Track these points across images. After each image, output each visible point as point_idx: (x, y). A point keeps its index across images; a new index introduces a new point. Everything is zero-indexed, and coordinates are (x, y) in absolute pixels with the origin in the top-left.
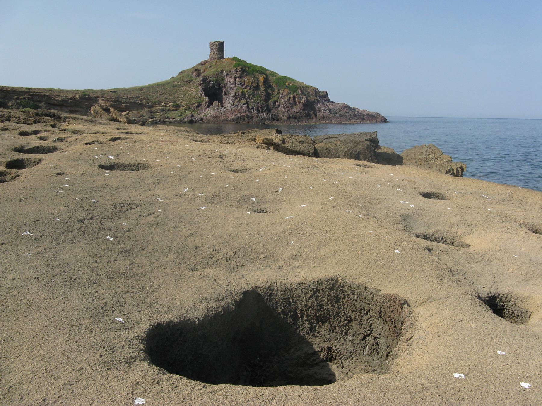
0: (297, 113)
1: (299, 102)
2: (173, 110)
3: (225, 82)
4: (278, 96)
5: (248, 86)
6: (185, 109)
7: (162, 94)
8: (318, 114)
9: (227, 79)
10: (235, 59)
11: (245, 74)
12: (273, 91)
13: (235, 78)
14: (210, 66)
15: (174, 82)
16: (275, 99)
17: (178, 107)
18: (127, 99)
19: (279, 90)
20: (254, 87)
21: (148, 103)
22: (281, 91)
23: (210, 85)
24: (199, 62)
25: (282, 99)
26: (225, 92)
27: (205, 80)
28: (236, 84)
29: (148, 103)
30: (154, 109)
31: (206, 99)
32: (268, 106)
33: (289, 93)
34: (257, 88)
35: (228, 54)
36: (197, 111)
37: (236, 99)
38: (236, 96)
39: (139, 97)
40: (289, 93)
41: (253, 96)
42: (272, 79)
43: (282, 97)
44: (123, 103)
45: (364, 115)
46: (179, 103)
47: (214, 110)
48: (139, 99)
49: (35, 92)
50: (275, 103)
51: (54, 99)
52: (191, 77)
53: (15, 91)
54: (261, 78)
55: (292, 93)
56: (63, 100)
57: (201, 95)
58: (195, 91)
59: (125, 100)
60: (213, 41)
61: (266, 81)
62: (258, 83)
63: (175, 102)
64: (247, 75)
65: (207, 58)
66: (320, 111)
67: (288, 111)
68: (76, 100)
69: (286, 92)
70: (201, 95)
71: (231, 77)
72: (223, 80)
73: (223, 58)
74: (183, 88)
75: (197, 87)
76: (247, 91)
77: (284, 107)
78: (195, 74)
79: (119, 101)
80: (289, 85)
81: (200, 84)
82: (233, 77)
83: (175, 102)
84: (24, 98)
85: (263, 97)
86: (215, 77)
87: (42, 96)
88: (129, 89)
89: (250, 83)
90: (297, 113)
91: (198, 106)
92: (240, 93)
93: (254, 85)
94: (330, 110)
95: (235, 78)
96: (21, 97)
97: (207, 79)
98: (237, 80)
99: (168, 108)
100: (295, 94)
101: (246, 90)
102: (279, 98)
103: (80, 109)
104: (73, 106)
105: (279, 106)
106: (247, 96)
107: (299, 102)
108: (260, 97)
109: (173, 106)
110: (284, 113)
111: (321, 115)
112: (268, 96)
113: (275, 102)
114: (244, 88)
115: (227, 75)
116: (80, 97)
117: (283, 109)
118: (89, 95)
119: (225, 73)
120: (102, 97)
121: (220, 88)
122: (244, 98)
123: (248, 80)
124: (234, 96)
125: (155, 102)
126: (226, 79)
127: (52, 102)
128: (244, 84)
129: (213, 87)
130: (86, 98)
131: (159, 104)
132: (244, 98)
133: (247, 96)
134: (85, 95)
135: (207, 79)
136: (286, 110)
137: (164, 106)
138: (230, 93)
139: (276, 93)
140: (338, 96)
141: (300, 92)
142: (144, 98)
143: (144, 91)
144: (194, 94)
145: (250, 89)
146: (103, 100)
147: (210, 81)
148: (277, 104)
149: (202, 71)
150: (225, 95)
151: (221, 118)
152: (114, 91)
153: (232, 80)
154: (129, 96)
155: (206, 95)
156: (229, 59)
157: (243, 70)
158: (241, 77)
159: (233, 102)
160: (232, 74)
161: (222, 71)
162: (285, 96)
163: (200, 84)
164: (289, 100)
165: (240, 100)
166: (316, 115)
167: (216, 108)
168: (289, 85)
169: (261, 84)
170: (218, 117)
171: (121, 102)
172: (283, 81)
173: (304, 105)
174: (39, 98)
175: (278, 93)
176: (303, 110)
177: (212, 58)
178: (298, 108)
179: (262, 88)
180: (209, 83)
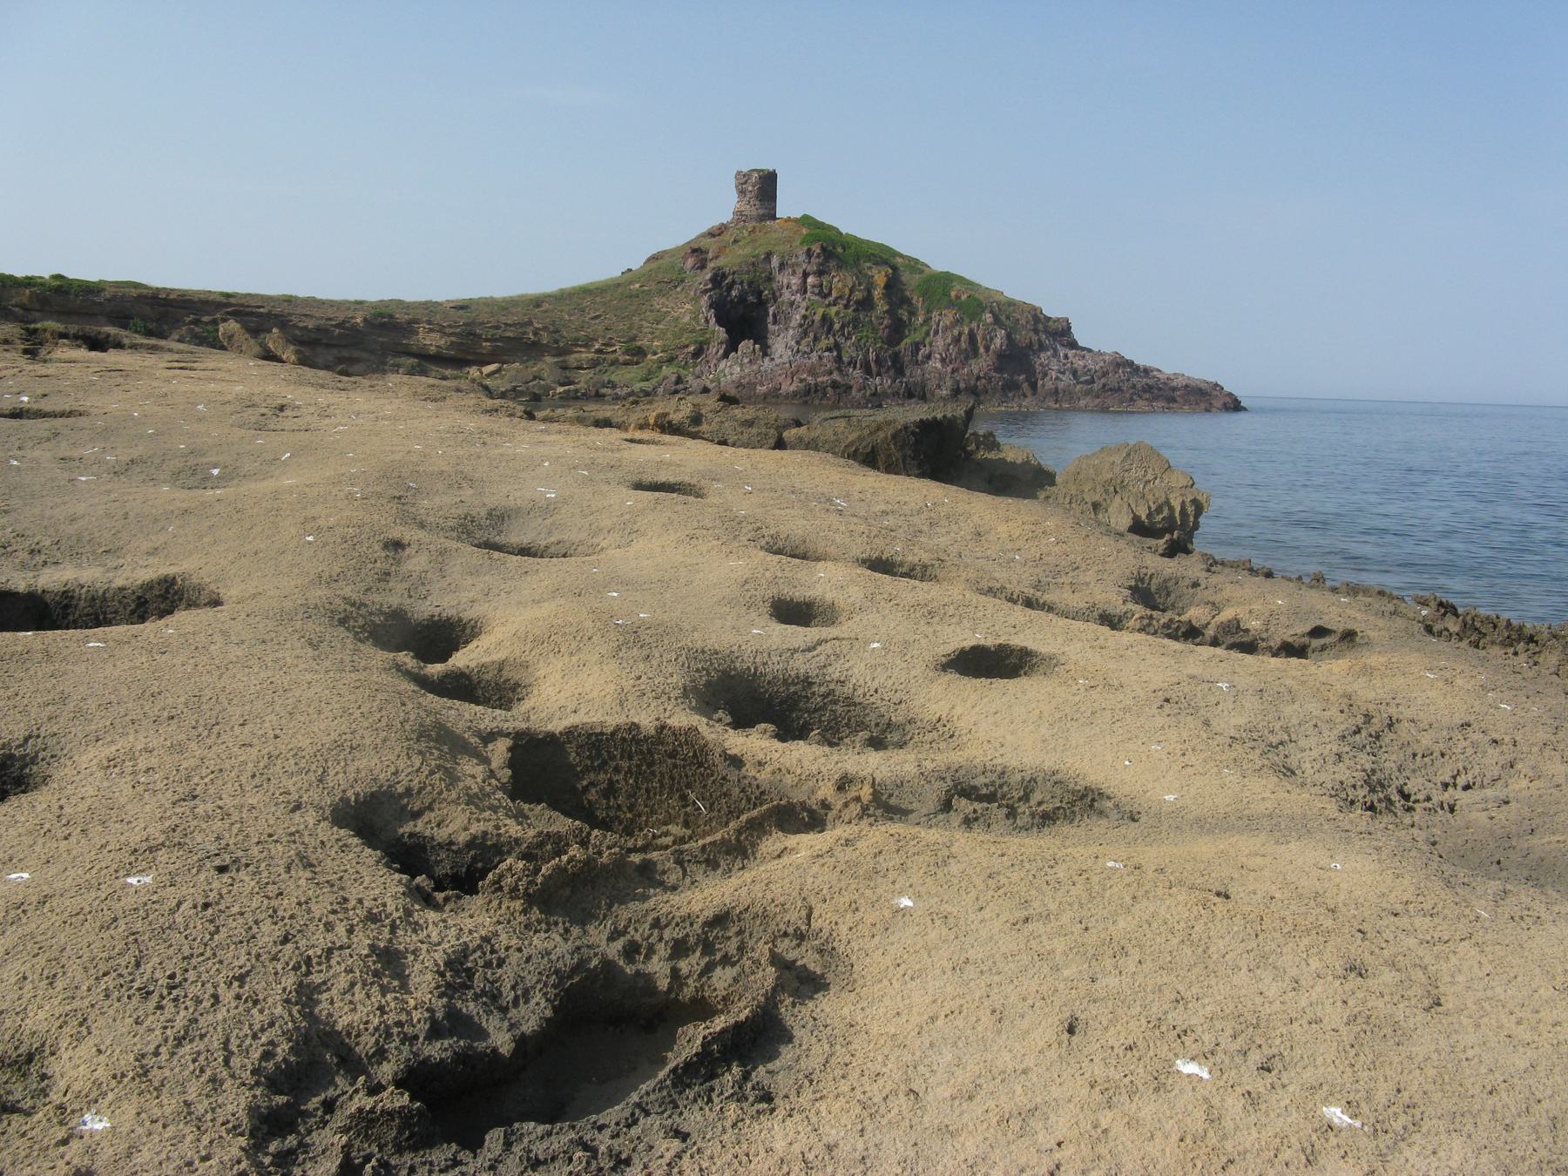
0: (978, 378)
1: (987, 349)
2: (626, 363)
3: (775, 286)
5: (841, 297)
6: (661, 362)
7: (597, 317)
8: (1040, 383)
9: (783, 278)
10: (807, 221)
11: (832, 264)
12: (912, 313)
13: (805, 275)
14: (735, 241)
15: (631, 283)
16: (917, 337)
17: (640, 353)
18: (497, 328)
19: (929, 311)
20: (857, 302)
21: (556, 342)
22: (935, 315)
23: (734, 293)
24: (705, 228)
26: (775, 316)
27: (718, 279)
29: (556, 342)
30: (572, 359)
31: (721, 333)
32: (896, 357)
33: (958, 322)
34: (866, 303)
35: (788, 205)
36: (695, 366)
37: (805, 334)
38: (805, 328)
39: (530, 323)
41: (855, 327)
42: (910, 280)
43: (936, 332)
44: (487, 340)
45: (1174, 389)
46: (643, 342)
47: (741, 365)
48: (529, 329)
50: (918, 350)
52: (681, 270)
53: (190, 301)
54: (880, 277)
55: (967, 321)
56: (318, 329)
57: (707, 321)
58: (690, 310)
59: (492, 331)
60: (745, 170)
61: (893, 285)
62: (869, 291)
63: (634, 339)
64: (839, 268)
68: (354, 327)
70: (707, 321)
71: (794, 273)
72: (770, 279)
73: (773, 217)
74: (658, 302)
75: (695, 300)
76: (837, 313)
77: (943, 360)
78: (690, 262)
79: (475, 335)
80: (958, 297)
81: (705, 292)
82: (800, 272)
86: (748, 272)
87: (260, 315)
88: (504, 300)
89: (847, 291)
90: (978, 378)
91: (696, 355)
92: (817, 318)
93: (858, 295)
94: (1075, 373)
95: (805, 275)
96: (206, 319)
97: (724, 276)
98: (810, 280)
99: (612, 357)
100: (974, 325)
101: (834, 310)
102: (928, 334)
103: (364, 355)
104: (345, 346)
105: (929, 357)
106: (837, 326)
107: (987, 349)
108: (875, 330)
109: (627, 352)
111: (1049, 385)
112: (898, 329)
113: (917, 347)
114: (829, 305)
115: (782, 266)
116: (365, 320)
117: (939, 365)
118: (391, 316)
119: (775, 262)
120: (429, 322)
121: (762, 304)
122: (828, 332)
123: (840, 281)
124: (801, 326)
125: (577, 339)
126: (779, 277)
128: (830, 294)
129: (742, 299)
130: (383, 325)
131: (585, 346)
132: (828, 332)
133: (837, 326)
134: (381, 315)
135: (724, 276)
136: (949, 369)
137: (599, 351)
138: (788, 319)
139: (921, 319)
140: (1098, 334)
142: (545, 328)
143: (546, 306)
145: (846, 307)
146: (431, 330)
147: (734, 282)
148: (923, 351)
149: (710, 255)
150: (775, 323)
151: (761, 389)
153: (795, 281)
154: (503, 319)
155: (719, 322)
156: (789, 219)
158: (820, 273)
159: (798, 343)
160: (798, 265)
161: (769, 256)
162: (946, 328)
163: (705, 292)
164: (957, 340)
165: (816, 339)
166: (1034, 386)
168: (958, 297)
170: (752, 385)
171: (479, 336)
172: (942, 286)
173: (1001, 356)
175: (927, 321)
176: (997, 370)
177: (740, 216)
178: (982, 364)
179: (882, 306)
180: (730, 287)
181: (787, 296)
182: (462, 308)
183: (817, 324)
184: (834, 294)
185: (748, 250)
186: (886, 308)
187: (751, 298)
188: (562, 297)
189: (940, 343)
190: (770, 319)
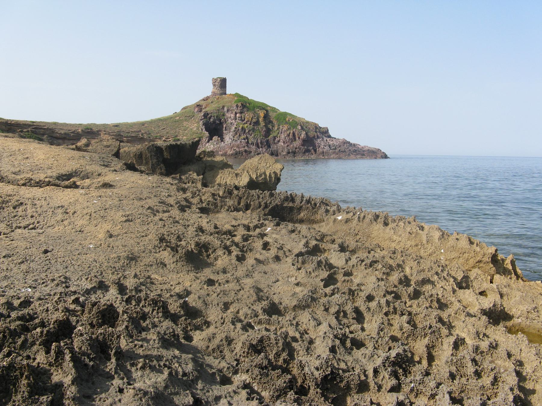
1: (299, 138)
4: (278, 131)
5: (248, 121)
7: (164, 129)
9: (228, 115)
10: (237, 95)
11: (245, 109)
12: (273, 126)
13: (236, 113)
15: (176, 117)
16: (275, 134)
19: (279, 125)
20: (254, 123)
21: (150, 137)
22: (281, 127)
23: (211, 120)
24: (201, 98)
25: (282, 135)
26: (226, 128)
27: (206, 115)
28: (236, 119)
32: (268, 141)
33: (289, 129)
34: (257, 123)
35: (230, 90)
38: (236, 131)
39: (140, 131)
40: (289, 129)
41: (253, 131)
42: (272, 115)
43: (282, 133)
44: (125, 137)
48: (140, 133)
49: (38, 126)
50: (275, 139)
51: (57, 133)
53: (19, 124)
54: (262, 114)
56: (65, 134)
57: (202, 130)
59: (127, 134)
60: (215, 78)
63: (177, 136)
64: (248, 111)
65: (209, 94)
66: (319, 147)
67: (287, 146)
69: (286, 127)
70: (202, 130)
71: (232, 113)
72: (224, 115)
74: (185, 124)
75: (198, 122)
76: (247, 127)
77: (284, 142)
78: (196, 109)
79: (121, 135)
80: (289, 120)
81: (201, 120)
82: (234, 112)
83: (177, 136)
84: (28, 131)
85: (263, 133)
86: (216, 113)
88: (131, 123)
90: (296, 148)
92: (240, 128)
94: (329, 146)
95: (236, 113)
97: (208, 114)
98: (238, 115)
100: (294, 130)
102: (278, 133)
105: (279, 141)
106: (247, 131)
107: (299, 138)
108: (260, 132)
110: (283, 148)
111: (321, 150)
112: (268, 132)
113: (275, 138)
115: (228, 111)
116: (82, 130)
117: (282, 144)
118: (91, 129)
119: (226, 109)
120: (105, 131)
121: (221, 124)
123: (248, 116)
124: (235, 131)
125: (157, 137)
126: (227, 114)
127: (55, 135)
128: (244, 120)
129: (214, 122)
131: (160, 139)
132: (244, 133)
133: (247, 131)
134: (88, 129)
135: (208, 114)
137: (165, 141)
138: (230, 129)
141: (299, 127)
143: (146, 125)
144: (195, 129)
145: (250, 124)
146: (105, 134)
147: (211, 116)
148: (277, 139)
150: (226, 130)
152: (117, 126)
153: (233, 116)
155: (206, 130)
156: (231, 95)
157: (243, 106)
159: (233, 137)
161: (223, 107)
162: (285, 131)
163: (201, 120)
164: (289, 135)
165: (240, 135)
166: (315, 151)
167: (215, 143)
168: (289, 120)
169: (261, 119)
171: (122, 136)
172: (283, 117)
174: (42, 131)
177: (214, 94)
178: (297, 143)
179: (262, 124)
180: (210, 118)
181: (230, 121)
182: (116, 126)
183: (240, 130)
184: (246, 120)
185: (216, 105)
186: (264, 124)
187: (217, 122)
188: (152, 122)
189: (283, 136)
190: (224, 129)
